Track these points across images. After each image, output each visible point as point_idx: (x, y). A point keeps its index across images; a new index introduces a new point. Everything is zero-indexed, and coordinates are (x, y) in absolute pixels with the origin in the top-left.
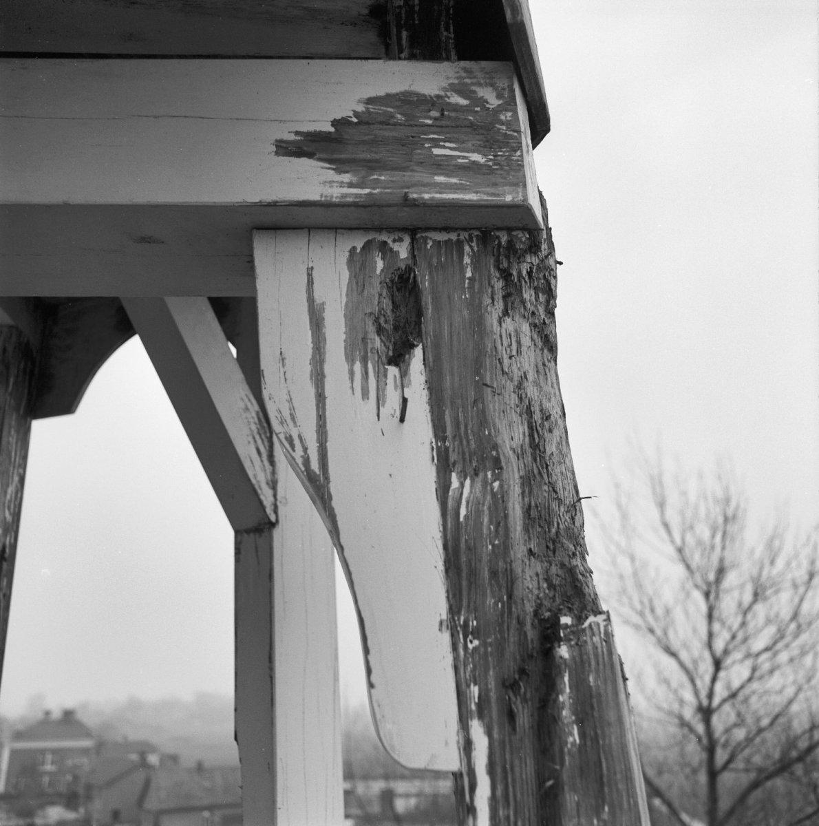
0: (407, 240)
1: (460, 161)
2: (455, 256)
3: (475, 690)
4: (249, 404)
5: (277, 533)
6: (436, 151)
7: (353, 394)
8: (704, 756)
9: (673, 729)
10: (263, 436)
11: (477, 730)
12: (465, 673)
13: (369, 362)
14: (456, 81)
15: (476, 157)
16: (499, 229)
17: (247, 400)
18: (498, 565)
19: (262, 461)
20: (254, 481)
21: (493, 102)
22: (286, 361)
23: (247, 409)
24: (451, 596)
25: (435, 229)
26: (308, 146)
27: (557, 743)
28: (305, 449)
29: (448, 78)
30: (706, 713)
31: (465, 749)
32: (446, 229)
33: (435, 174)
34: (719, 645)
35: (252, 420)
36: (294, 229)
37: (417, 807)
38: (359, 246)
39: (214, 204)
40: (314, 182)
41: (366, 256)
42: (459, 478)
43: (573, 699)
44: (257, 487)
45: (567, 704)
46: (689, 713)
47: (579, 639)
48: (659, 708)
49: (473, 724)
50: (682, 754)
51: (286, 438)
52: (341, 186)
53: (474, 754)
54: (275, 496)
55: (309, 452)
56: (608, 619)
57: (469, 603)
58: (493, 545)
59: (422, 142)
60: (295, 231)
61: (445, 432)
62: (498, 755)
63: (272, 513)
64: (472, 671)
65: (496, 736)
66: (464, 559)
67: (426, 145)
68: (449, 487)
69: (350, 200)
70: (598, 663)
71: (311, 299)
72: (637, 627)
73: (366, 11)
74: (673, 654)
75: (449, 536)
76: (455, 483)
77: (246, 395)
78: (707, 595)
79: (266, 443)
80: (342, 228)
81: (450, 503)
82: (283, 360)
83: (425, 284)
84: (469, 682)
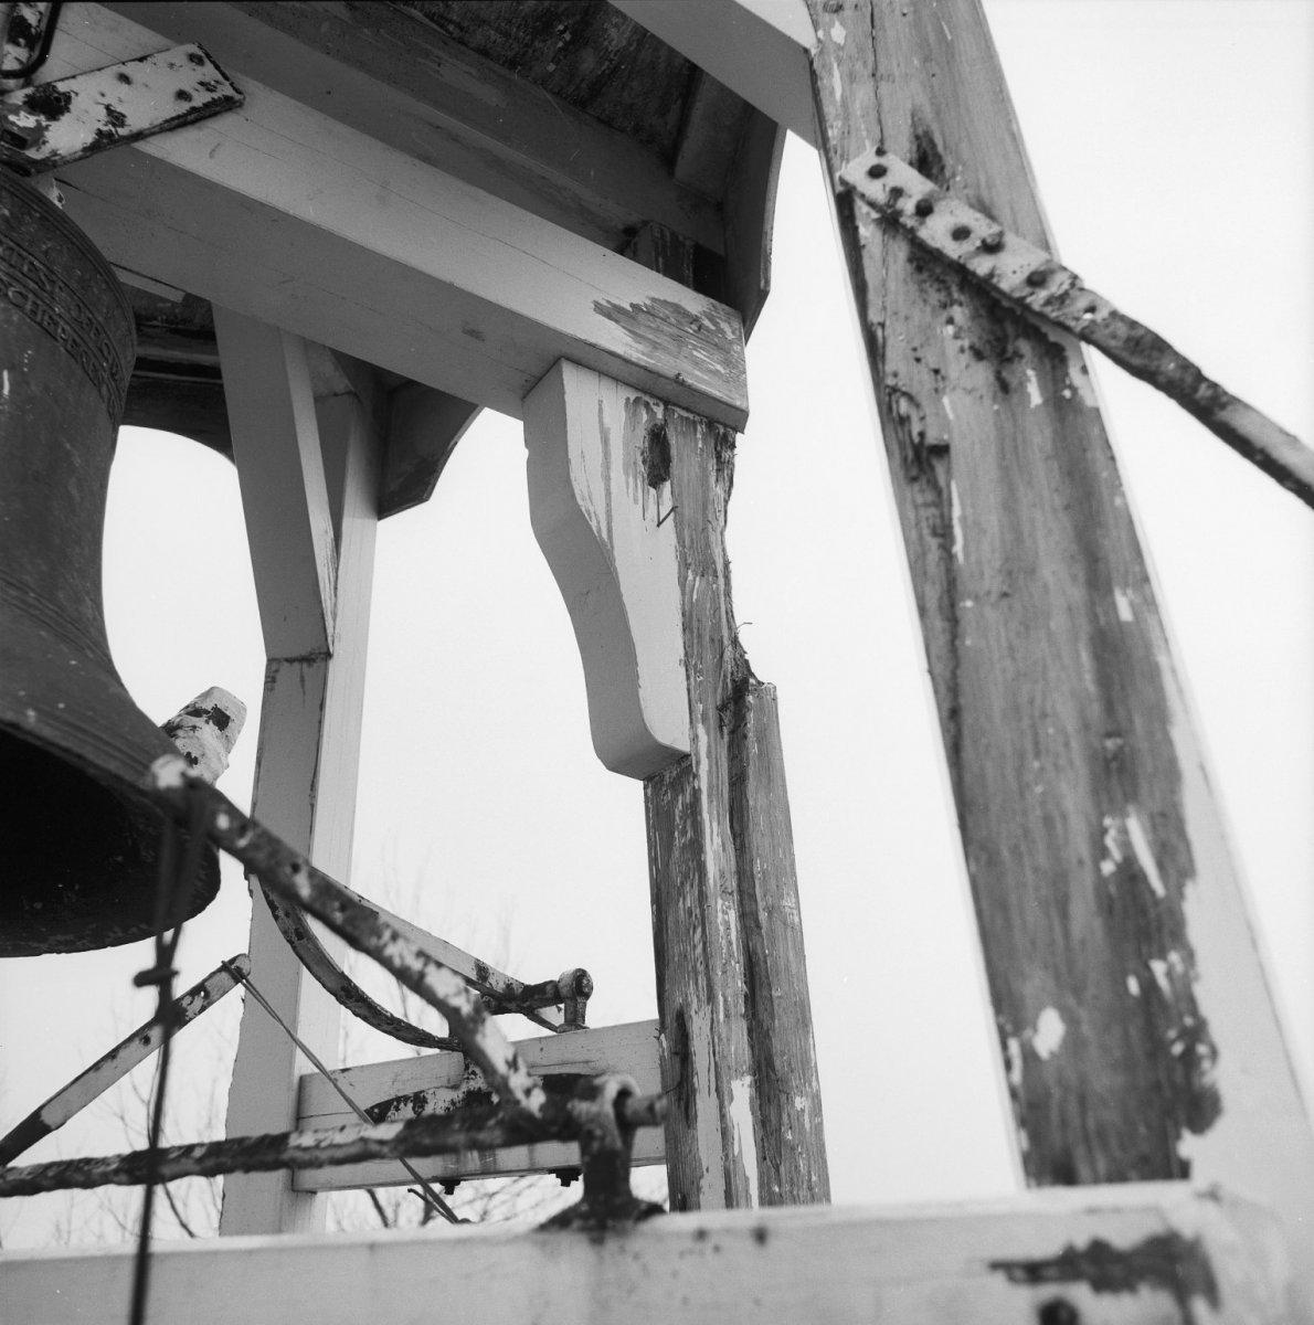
0: (662, 407)
5: (332, 664)
6: (695, 353)
11: (701, 730)
15: (719, 367)
16: (718, 422)
21: (730, 336)
23: (326, 532)
25: (680, 407)
26: (612, 312)
27: (745, 753)
28: (598, 523)
32: (687, 409)
37: (1034, 369)
38: (632, 399)
40: (614, 338)
73: (621, 227)
76: (690, 577)
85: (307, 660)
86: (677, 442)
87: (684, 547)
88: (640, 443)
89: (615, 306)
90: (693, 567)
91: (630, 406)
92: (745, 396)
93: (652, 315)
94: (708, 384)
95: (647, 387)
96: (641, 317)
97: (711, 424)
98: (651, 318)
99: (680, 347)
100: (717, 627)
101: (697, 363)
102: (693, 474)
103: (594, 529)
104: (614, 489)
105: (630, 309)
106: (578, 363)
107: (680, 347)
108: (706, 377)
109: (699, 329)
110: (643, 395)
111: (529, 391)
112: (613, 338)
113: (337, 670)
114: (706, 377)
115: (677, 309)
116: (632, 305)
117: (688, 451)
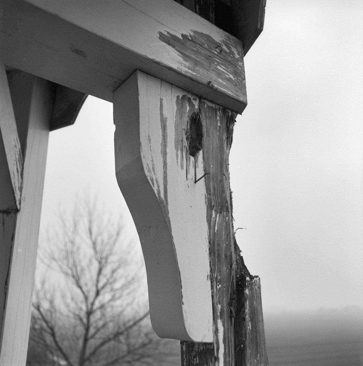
0: (198, 101)
1: (226, 75)
2: (214, 115)
3: (219, 306)
4: (17, 145)
5: (19, 215)
6: (219, 67)
7: (178, 165)
8: (84, 332)
9: (72, 320)
10: (20, 163)
12: (216, 299)
13: (184, 152)
14: (225, 40)
15: (231, 76)
16: (229, 109)
17: (16, 142)
18: (227, 253)
19: (18, 176)
20: (13, 186)
22: (151, 141)
23: (16, 146)
24: (211, 265)
25: (208, 100)
26: (169, 40)
28: (158, 187)
29: (222, 37)
30: (89, 313)
31: (215, 332)
32: (212, 102)
33: (219, 78)
34: (101, 284)
35: (17, 153)
36: (155, 77)
38: (181, 96)
39: (132, 51)
40: (171, 58)
41: (183, 101)
42: (215, 213)
43: (250, 311)
44: (14, 189)
45: (248, 313)
46: (83, 314)
47: (251, 287)
48: (69, 311)
49: (219, 322)
50: (74, 332)
51: (150, 179)
52: (185, 67)
53: (219, 334)
54: (21, 195)
55: (160, 188)
56: (259, 280)
57: (218, 269)
58: (226, 244)
59: (214, 61)
60: (155, 78)
61: (211, 192)
62: (227, 335)
63: (19, 205)
64: (218, 298)
65: (226, 327)
66: (216, 249)
67: (216, 63)
68: (212, 216)
69: (189, 75)
70: (257, 297)
71: (162, 114)
72: (67, 274)
74: (80, 288)
75: (211, 238)
76: (214, 216)
77: (17, 139)
78: (100, 263)
79: (21, 167)
80: (174, 85)
81: (212, 225)
82: (150, 140)
83: (204, 123)
84: (217, 303)
85: (6, 212)
86: (206, 123)
87: (210, 194)
88: (185, 127)
89: (172, 36)
90: (215, 208)
91: (179, 101)
92: (245, 94)
93: (194, 42)
94: (225, 87)
95: (190, 89)
96: (188, 44)
97: (224, 110)
98: (194, 44)
99: (210, 63)
100: (228, 247)
101: (219, 74)
102: (215, 144)
103: (156, 192)
104: (168, 161)
105: (182, 38)
106: (148, 73)
107: (210, 63)
108: (224, 83)
109: (221, 52)
110: (187, 94)
111: (119, 86)
112: (171, 58)
113: (22, 219)
114: (224, 83)
115: (208, 38)
116: (183, 35)
117: (211, 127)
